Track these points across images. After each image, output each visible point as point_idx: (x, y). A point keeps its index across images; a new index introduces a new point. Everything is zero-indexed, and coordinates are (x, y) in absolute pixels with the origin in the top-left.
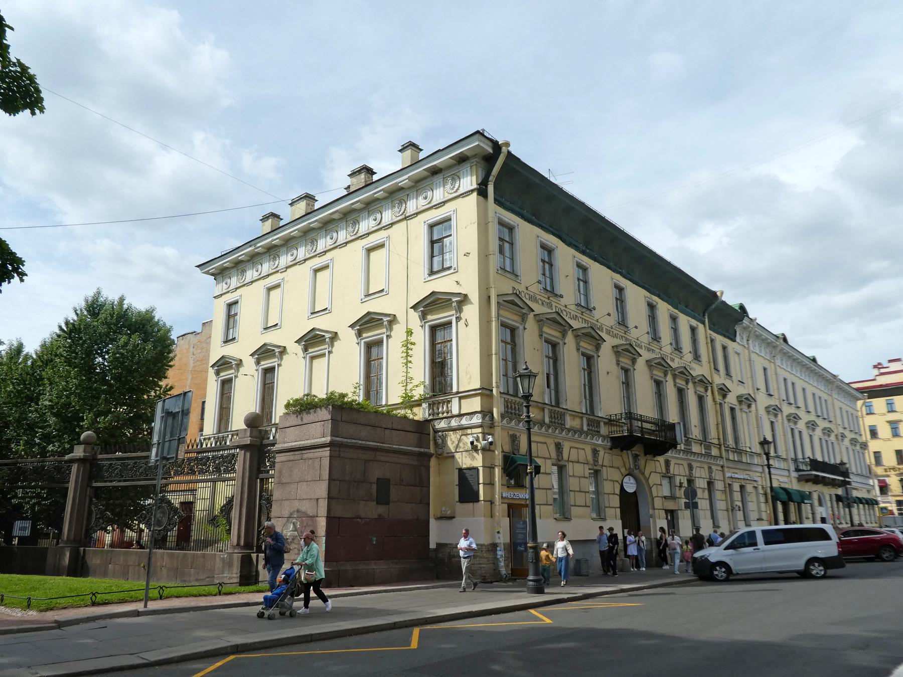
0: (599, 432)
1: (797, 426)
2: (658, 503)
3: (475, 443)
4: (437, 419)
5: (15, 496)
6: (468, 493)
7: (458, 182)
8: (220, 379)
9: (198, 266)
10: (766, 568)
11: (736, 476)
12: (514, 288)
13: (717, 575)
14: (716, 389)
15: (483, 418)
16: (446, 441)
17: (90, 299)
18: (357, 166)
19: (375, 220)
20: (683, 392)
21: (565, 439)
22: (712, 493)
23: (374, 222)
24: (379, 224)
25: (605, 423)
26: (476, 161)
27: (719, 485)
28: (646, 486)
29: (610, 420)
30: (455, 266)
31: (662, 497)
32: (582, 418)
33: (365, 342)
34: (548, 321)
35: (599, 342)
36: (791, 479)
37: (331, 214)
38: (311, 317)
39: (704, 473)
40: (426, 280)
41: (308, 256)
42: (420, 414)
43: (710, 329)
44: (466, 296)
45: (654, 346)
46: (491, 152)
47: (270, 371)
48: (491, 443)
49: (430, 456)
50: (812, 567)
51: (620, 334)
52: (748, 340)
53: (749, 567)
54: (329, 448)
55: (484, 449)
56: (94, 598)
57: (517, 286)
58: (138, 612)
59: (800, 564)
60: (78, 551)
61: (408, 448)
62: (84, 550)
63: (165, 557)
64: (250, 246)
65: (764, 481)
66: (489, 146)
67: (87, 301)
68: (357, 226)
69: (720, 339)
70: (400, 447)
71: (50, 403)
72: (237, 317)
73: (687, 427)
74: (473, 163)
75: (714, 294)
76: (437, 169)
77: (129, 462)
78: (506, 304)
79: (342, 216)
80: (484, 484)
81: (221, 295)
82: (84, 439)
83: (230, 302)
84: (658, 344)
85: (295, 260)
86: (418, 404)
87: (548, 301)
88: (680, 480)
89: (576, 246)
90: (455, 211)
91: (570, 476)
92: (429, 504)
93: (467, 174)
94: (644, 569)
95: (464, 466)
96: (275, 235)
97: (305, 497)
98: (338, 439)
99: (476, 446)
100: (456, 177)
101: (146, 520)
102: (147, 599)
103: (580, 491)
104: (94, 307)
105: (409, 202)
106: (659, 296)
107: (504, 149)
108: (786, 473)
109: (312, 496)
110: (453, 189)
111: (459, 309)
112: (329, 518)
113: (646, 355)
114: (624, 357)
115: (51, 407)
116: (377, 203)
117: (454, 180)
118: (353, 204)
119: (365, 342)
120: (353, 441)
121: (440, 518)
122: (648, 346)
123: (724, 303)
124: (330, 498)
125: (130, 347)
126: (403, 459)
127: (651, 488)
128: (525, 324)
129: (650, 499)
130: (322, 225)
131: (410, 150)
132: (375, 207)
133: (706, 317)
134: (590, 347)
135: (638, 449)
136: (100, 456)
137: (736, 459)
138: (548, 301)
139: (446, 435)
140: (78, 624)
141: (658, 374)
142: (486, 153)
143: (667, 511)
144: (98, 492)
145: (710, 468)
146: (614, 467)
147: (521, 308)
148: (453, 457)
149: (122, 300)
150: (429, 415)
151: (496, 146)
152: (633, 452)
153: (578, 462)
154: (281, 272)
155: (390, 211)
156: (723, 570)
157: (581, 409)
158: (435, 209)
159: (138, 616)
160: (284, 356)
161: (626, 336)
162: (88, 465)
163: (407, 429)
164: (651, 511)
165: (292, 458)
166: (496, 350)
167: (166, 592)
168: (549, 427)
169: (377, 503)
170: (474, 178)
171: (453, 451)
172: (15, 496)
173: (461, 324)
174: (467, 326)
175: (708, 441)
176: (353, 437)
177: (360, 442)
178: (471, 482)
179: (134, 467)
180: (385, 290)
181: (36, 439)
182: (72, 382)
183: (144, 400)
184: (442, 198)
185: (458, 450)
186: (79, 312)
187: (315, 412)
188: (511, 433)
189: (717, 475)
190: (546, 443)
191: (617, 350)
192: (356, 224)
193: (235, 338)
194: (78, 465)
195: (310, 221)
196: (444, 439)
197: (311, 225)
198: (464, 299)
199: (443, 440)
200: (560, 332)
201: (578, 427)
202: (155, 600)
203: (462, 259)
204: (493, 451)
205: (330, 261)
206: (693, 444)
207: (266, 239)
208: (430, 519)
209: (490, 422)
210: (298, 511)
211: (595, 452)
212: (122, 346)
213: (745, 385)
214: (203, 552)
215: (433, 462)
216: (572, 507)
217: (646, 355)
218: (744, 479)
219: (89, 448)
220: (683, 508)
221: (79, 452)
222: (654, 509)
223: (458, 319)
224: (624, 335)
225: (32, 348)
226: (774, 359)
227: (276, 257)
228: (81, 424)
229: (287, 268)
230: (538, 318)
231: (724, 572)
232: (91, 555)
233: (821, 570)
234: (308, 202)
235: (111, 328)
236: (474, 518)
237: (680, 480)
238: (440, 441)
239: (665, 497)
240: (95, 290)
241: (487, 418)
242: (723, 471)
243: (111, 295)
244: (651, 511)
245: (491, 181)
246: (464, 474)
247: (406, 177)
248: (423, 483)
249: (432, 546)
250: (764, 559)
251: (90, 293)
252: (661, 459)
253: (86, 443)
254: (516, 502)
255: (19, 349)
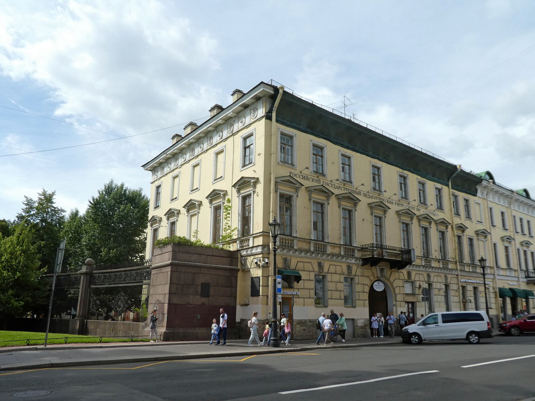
0: (354, 255)
1: (529, 249)
2: (399, 298)
3: (259, 263)
4: (242, 250)
5: (70, 293)
6: (255, 292)
7: (257, 112)
8: (153, 228)
9: (142, 166)
10: (443, 337)
11: (470, 281)
12: (291, 173)
13: (413, 340)
14: (454, 227)
15: (263, 249)
16: (247, 262)
17: (107, 186)
18: (213, 105)
19: (219, 136)
20: (427, 230)
21: (324, 260)
22: (448, 292)
23: (219, 138)
24: (221, 138)
25: (358, 250)
26: (265, 99)
27: (453, 287)
28: (391, 288)
29: (362, 248)
30: (254, 162)
31: (403, 294)
32: (340, 247)
33: (213, 207)
34: (316, 191)
35: (356, 201)
36: (520, 283)
37: (199, 134)
38: (191, 193)
39: (442, 279)
40: (241, 170)
41: (191, 158)
42: (233, 247)
43: (452, 188)
44: (258, 178)
45: (403, 202)
46: (273, 93)
47: (173, 224)
48: (267, 263)
49: (238, 270)
50: (470, 337)
51: (375, 195)
52: (487, 195)
53: (432, 336)
54: (170, 267)
55: (263, 267)
56: (28, 342)
57: (293, 171)
58: (37, 348)
59: (464, 335)
60: (84, 322)
61: (223, 266)
62: (87, 321)
63: (121, 325)
64: (164, 154)
65: (495, 284)
66: (271, 90)
67: (105, 187)
68: (212, 140)
69: (462, 196)
70: (217, 266)
71: (86, 244)
72: (160, 194)
73: (429, 251)
74: (263, 100)
75: (455, 167)
76: (246, 105)
77: (117, 273)
78: (282, 182)
79: (204, 135)
80: (262, 286)
81: (154, 182)
82: (87, 262)
83: (158, 186)
84: (407, 201)
85: (185, 160)
86: (234, 241)
87: (318, 179)
88: (420, 283)
89: (341, 144)
90: (255, 129)
91: (328, 281)
92: (236, 297)
93: (261, 108)
94: (382, 336)
95: (254, 276)
96: (175, 147)
97: (161, 293)
98: (176, 261)
99: (259, 265)
100: (256, 109)
101: (114, 305)
102: (46, 344)
103: (336, 290)
104: (109, 190)
105: (234, 125)
106: (409, 171)
107: (281, 91)
108: (516, 279)
109: (164, 293)
110: (254, 116)
111: (255, 187)
112: (170, 304)
113: (394, 208)
114: (375, 209)
115: (86, 245)
116: (221, 126)
117: (254, 111)
118: (208, 128)
119: (213, 207)
120: (186, 262)
121: (242, 305)
122: (398, 202)
123: (462, 171)
124: (170, 293)
125: (126, 211)
126: (220, 273)
127: (394, 289)
128: (298, 193)
129: (394, 295)
130: (196, 140)
131: (236, 94)
132: (220, 128)
133: (450, 182)
134: (349, 205)
135: (382, 264)
136: (94, 272)
137: (471, 270)
138: (318, 179)
139: (246, 259)
140: (3, 353)
141: (407, 220)
142: (270, 94)
143: (408, 303)
144: (97, 292)
145: (446, 276)
146: (364, 276)
147: (295, 184)
148: (249, 271)
149: (122, 186)
150: (240, 247)
151: (276, 90)
152: (380, 267)
153: (336, 273)
154: (179, 168)
155: (226, 130)
156: (417, 337)
157: (340, 242)
158: (246, 128)
159: (37, 350)
160: (179, 216)
161: (380, 197)
162: (89, 277)
163: (222, 256)
164: (394, 303)
165: (157, 272)
166: (272, 210)
167: (69, 340)
168: (313, 253)
169: (201, 296)
170: (264, 109)
171: (249, 267)
172: (70, 293)
173: (255, 195)
174: (258, 196)
175: (446, 260)
176: (186, 260)
177: (190, 263)
178: (256, 285)
179: (109, 277)
180: (223, 177)
181: (79, 263)
182: (96, 231)
183: (137, 241)
184: (249, 122)
185: (251, 267)
186: (101, 193)
187: (167, 247)
188: (284, 257)
189: (451, 279)
190: (311, 263)
191: (371, 206)
192: (211, 139)
193: (159, 206)
194: (84, 277)
195: (189, 139)
196: (245, 260)
197: (190, 141)
198: (257, 180)
199: (245, 262)
200: (326, 197)
201: (337, 253)
202: (63, 344)
203: (257, 157)
204: (269, 267)
205: (200, 161)
206: (432, 262)
207: (171, 150)
208: (237, 306)
209: (267, 251)
210: (158, 300)
211: (349, 268)
212: (122, 211)
213: (483, 224)
214: (129, 322)
215: (240, 274)
216: (435, 303)
217: (394, 208)
218: (477, 283)
219: (89, 267)
220: (421, 301)
221: (84, 269)
222: (396, 301)
223: (254, 192)
224: (378, 196)
225: (82, 212)
226: (510, 206)
227: (177, 159)
228: (101, 254)
229: (182, 165)
230: (308, 189)
231: (417, 339)
232: (90, 324)
233: (476, 339)
234: (192, 127)
235: (117, 201)
236: (257, 305)
237: (420, 283)
238: (243, 262)
239: (406, 294)
240: (110, 180)
241: (266, 249)
242: (457, 278)
243: (118, 183)
244: (394, 303)
245: (274, 111)
246: (254, 280)
247: (231, 111)
248: (234, 286)
249: (238, 320)
250: (441, 332)
251: (107, 182)
252: (404, 271)
253: (88, 264)
254: (286, 296)
255: (77, 213)
